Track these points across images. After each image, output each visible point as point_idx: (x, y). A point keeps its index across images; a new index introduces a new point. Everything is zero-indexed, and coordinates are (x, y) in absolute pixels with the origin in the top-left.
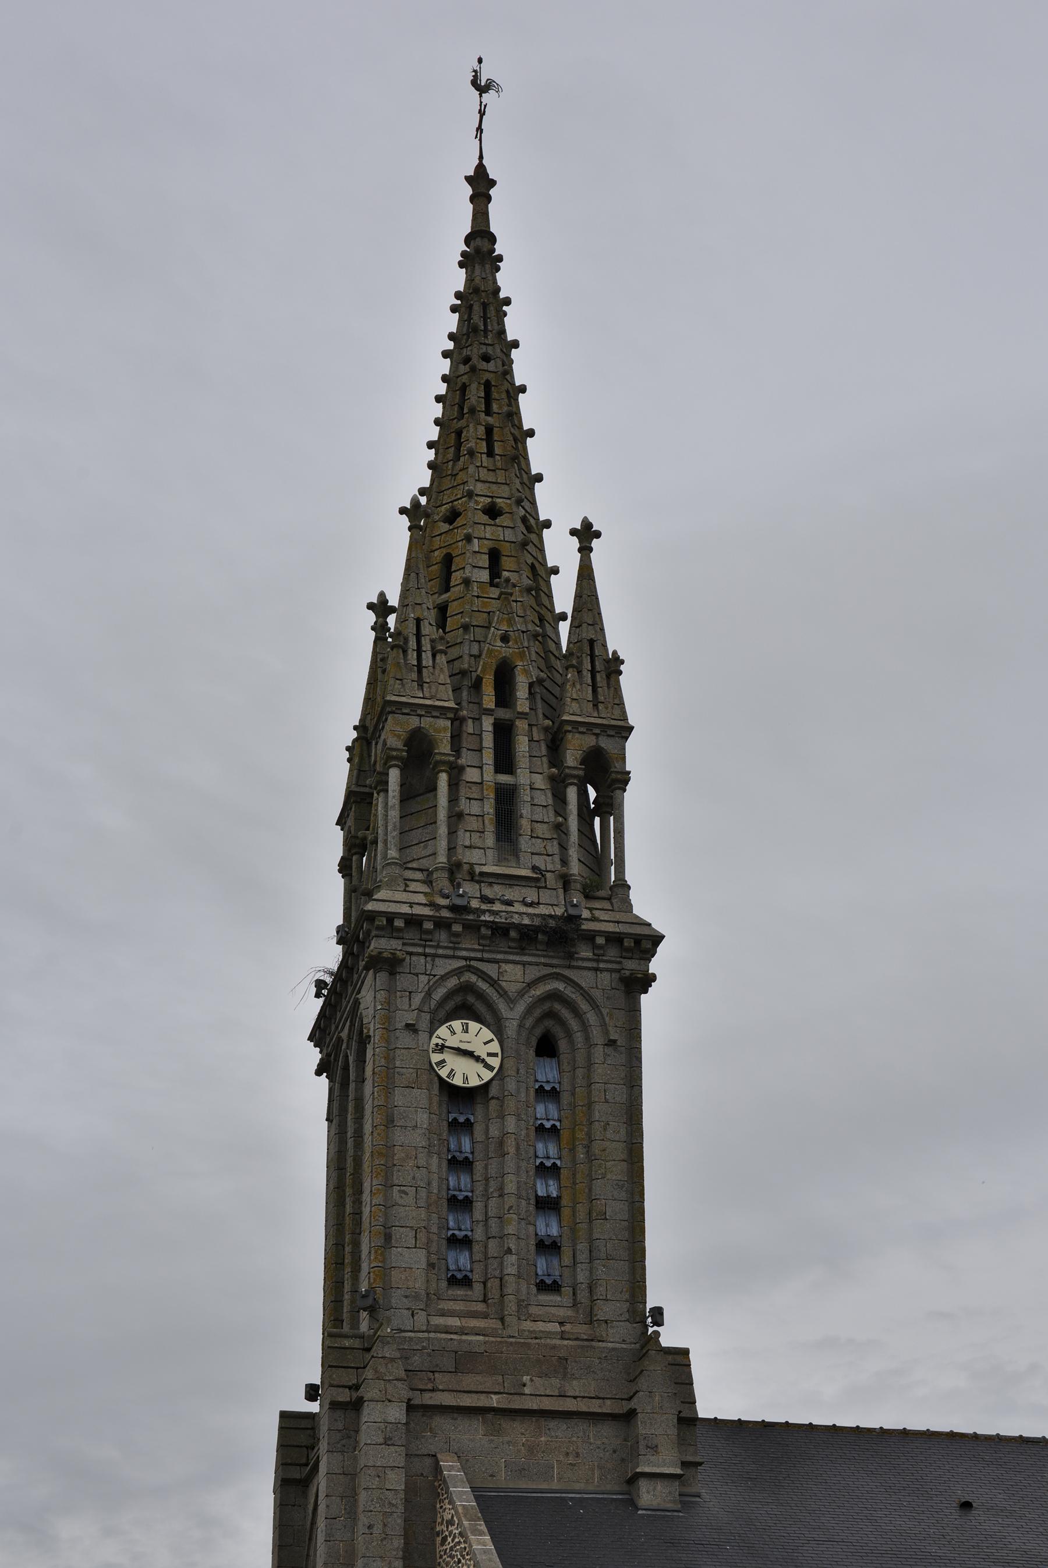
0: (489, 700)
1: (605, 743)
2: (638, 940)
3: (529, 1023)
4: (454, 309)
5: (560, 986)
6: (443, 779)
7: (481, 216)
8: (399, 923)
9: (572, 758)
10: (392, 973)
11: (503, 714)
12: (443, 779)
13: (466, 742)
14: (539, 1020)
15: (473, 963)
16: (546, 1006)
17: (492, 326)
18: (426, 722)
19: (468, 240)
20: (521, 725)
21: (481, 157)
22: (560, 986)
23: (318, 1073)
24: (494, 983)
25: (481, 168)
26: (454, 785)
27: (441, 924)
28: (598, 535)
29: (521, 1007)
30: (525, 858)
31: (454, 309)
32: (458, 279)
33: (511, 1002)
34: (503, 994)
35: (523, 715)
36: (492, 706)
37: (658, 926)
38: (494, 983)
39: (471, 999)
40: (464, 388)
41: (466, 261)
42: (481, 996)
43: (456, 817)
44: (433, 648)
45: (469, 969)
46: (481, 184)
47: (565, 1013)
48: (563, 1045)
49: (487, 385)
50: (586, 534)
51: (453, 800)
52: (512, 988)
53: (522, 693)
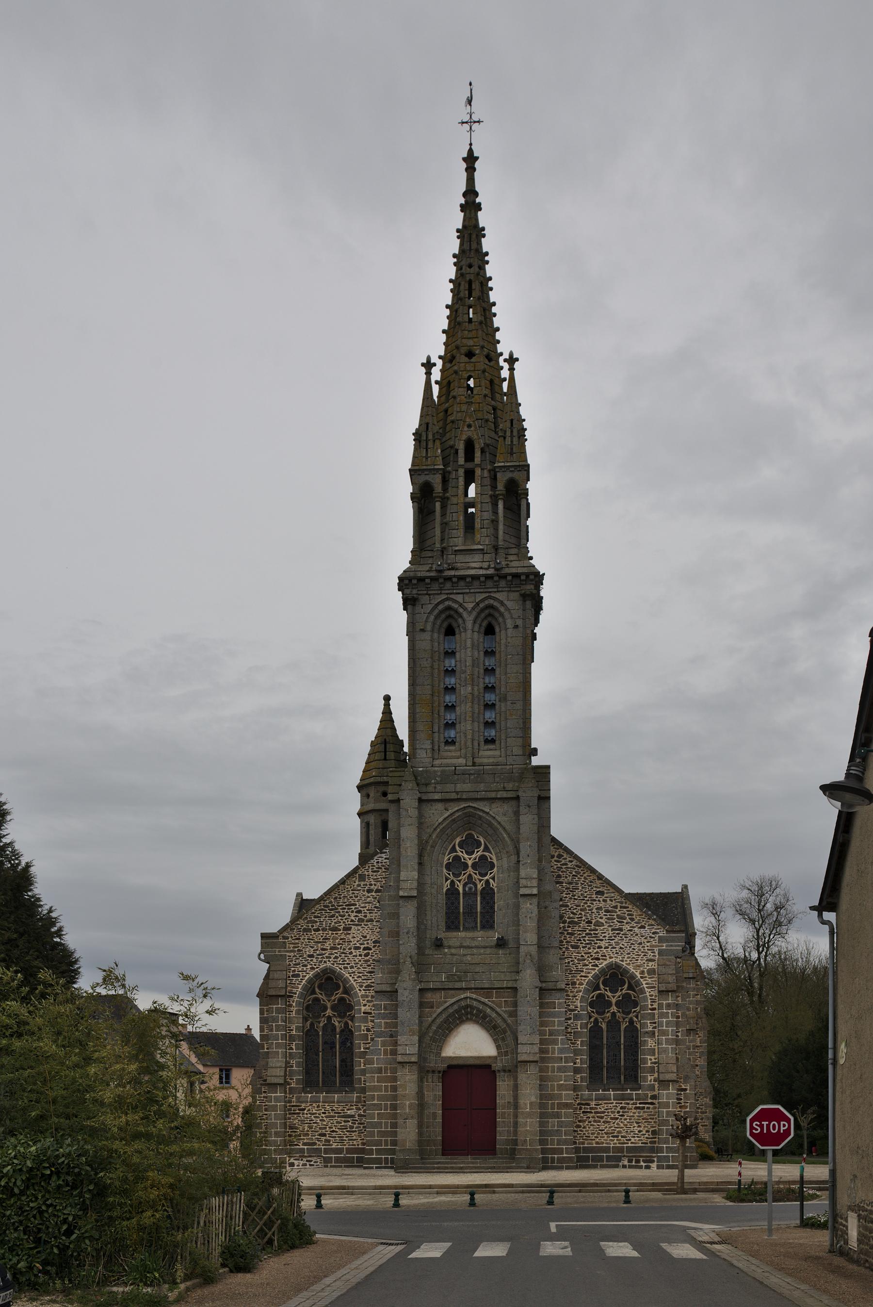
0: (461, 460)
1: (516, 475)
4: (487, 254)
5: (491, 602)
7: (471, 180)
8: (415, 581)
9: (500, 486)
10: (414, 605)
11: (470, 465)
13: (452, 483)
14: (486, 618)
15: (451, 596)
16: (487, 612)
17: (474, 246)
18: (429, 478)
19: (464, 195)
21: (471, 144)
23: (544, 574)
24: (461, 605)
25: (471, 151)
26: (444, 507)
27: (433, 579)
28: (517, 360)
30: (478, 536)
31: (487, 254)
32: (458, 219)
33: (470, 613)
34: (465, 609)
36: (463, 463)
38: (461, 605)
39: (452, 613)
40: (459, 284)
42: (456, 611)
43: (445, 525)
44: (433, 437)
45: (447, 599)
46: (471, 160)
48: (497, 630)
49: (470, 283)
50: (512, 360)
51: (443, 515)
53: (478, 454)
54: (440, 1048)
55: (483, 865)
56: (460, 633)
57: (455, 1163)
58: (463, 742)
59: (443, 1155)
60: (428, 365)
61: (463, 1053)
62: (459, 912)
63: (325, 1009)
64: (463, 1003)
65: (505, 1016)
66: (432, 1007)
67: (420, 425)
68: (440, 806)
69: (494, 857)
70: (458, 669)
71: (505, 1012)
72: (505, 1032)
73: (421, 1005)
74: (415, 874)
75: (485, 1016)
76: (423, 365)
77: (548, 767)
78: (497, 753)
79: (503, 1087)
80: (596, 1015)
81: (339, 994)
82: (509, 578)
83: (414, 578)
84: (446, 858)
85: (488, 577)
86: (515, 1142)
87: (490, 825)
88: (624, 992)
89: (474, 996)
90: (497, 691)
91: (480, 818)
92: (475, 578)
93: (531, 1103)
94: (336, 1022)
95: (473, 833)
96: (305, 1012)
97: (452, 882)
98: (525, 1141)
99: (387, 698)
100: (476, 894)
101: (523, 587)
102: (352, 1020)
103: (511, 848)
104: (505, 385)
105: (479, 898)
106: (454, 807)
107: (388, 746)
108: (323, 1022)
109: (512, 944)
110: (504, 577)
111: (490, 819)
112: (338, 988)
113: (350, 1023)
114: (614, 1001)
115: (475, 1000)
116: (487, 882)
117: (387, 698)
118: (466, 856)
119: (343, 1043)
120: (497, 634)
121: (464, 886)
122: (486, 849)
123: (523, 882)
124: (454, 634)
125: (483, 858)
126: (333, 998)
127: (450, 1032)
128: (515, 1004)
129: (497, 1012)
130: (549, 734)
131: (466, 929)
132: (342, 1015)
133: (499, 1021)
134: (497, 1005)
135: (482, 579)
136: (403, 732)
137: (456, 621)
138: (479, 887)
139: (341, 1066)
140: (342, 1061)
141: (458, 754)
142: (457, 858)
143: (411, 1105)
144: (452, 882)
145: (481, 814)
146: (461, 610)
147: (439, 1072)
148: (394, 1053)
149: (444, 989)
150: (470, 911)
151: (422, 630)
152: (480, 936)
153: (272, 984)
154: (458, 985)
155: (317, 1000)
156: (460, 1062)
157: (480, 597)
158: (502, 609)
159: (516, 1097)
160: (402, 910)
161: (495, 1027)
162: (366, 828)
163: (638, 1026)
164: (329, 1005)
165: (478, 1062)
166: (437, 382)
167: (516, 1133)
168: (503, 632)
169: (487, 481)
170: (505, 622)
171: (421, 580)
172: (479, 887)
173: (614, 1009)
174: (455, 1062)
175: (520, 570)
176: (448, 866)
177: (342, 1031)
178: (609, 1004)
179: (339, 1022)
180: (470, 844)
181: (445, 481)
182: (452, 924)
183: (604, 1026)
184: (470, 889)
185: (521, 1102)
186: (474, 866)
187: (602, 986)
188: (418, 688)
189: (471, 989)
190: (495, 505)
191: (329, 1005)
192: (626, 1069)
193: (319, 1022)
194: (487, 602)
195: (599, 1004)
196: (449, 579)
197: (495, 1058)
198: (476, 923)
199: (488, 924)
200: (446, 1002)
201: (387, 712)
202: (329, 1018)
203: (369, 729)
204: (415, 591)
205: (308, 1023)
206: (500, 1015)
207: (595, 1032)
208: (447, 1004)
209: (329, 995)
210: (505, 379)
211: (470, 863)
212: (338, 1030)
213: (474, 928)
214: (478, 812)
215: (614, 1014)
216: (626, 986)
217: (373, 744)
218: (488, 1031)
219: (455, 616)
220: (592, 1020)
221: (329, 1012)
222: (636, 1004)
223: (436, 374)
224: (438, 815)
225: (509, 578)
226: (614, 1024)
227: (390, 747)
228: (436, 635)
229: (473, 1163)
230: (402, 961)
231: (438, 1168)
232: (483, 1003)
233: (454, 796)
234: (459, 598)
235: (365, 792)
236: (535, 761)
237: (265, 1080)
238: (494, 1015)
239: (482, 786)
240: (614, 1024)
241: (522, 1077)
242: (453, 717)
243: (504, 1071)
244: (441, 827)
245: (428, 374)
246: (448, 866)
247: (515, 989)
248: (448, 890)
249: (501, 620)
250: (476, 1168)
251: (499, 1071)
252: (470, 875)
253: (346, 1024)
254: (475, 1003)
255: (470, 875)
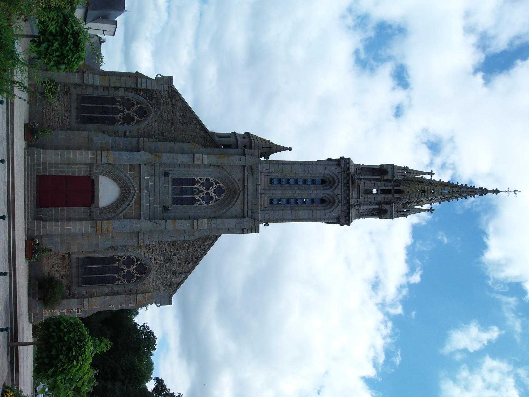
0: (395, 188)
1: (388, 214)
2: (348, 220)
3: (328, 177)
5: (337, 202)
6: (378, 177)
10: (337, 165)
12: (378, 177)
13: (386, 183)
14: (330, 200)
16: (332, 200)
19: (485, 189)
20: (390, 196)
22: (337, 202)
24: (336, 188)
25: (499, 192)
29: (332, 194)
30: (364, 195)
34: (334, 190)
35: (393, 196)
37: (351, 225)
38: (336, 188)
39: (332, 183)
41: (481, 189)
42: (333, 185)
45: (339, 182)
47: (331, 205)
48: (323, 205)
51: (374, 180)
52: (335, 192)
54: (105, 175)
55: (208, 199)
56: (323, 187)
57: (31, 184)
58: (271, 188)
59: (37, 176)
60: (431, 173)
61: (101, 188)
62: (182, 185)
63: (128, 110)
64: (132, 188)
65: (124, 212)
66: (130, 171)
67: (410, 170)
68: (241, 176)
69: (212, 204)
70: (306, 186)
71: (126, 212)
72: (114, 212)
73: (131, 165)
74: (205, 162)
75: (123, 200)
76: (432, 171)
77: (258, 232)
78: (266, 206)
79: (80, 211)
80: (122, 260)
81: (137, 118)
82: (347, 211)
83: (349, 166)
84: (212, 179)
85: (348, 201)
86: (45, 220)
87: (230, 202)
88: (136, 275)
89: (136, 195)
90: (295, 205)
91: (234, 197)
92: (348, 195)
93: (70, 229)
94: (121, 115)
95: (225, 193)
96: (127, 98)
97: (198, 182)
98: (46, 226)
99: (290, 149)
100: (192, 194)
101: (343, 218)
102: (121, 124)
103: (218, 214)
104: (419, 207)
105: (190, 196)
106: (240, 184)
107: (268, 149)
108: (121, 108)
109: (166, 215)
110: (348, 209)
111: (233, 202)
112: (141, 117)
113: (120, 123)
114: (131, 269)
115: (134, 196)
116: (199, 201)
117: (290, 149)
118: (213, 189)
119: (107, 118)
120: (322, 205)
121: (197, 188)
122: (217, 200)
123: (200, 221)
124: (322, 184)
125: (212, 198)
126: (134, 114)
127: (115, 181)
128: (130, 219)
129: (126, 208)
130: (272, 232)
131: (173, 189)
132: (124, 119)
133: (121, 209)
134: (130, 208)
135: (348, 198)
136: (273, 157)
137: (329, 185)
138: (196, 197)
139: (94, 116)
140: (97, 118)
141: (266, 186)
142: (212, 185)
143: (69, 158)
144: (198, 182)
145: (236, 198)
146: (334, 188)
147: (90, 174)
148: (102, 149)
149: (140, 178)
150: (182, 192)
151: (326, 169)
152: (169, 198)
153: (144, 80)
154: (142, 186)
155: (133, 105)
156: (95, 187)
157: (339, 196)
158: (333, 208)
159: (74, 220)
160: (186, 155)
161: (117, 207)
162: (227, 136)
163: (116, 283)
164: (130, 112)
165: (96, 196)
166: (422, 177)
167: (51, 220)
168: (322, 208)
169: (386, 200)
170: (327, 209)
171: (348, 169)
172: (196, 197)
173: (126, 270)
174: (95, 183)
175: (350, 216)
176: (208, 180)
177: (115, 118)
178: (129, 267)
179: (120, 117)
180: (219, 191)
181: (387, 180)
182: (176, 182)
183: (116, 265)
184: (195, 191)
185: (71, 223)
186: (208, 194)
187: (139, 262)
188: (299, 166)
189: (140, 193)
190: (377, 204)
191: (130, 112)
192: (90, 278)
193: (120, 106)
194: (337, 200)
195: (129, 262)
196: (348, 183)
197: (98, 206)
198: (176, 195)
199: (176, 201)
200: (133, 179)
201: (283, 149)
202: (123, 112)
203: (275, 140)
204: (343, 165)
205: (120, 100)
206: (124, 209)
207: (113, 260)
208: (131, 180)
209: (136, 112)
210: (422, 206)
211: (209, 191)
212: (115, 116)
213: (174, 194)
214: (237, 196)
215: (123, 270)
216: (139, 276)
217: (269, 141)
218: (115, 202)
219: (331, 185)
220: (120, 258)
221: (126, 111)
222: (129, 281)
223: (428, 177)
224: (237, 175)
225: (347, 211)
226: (117, 270)
227: (268, 150)
228: (323, 175)
229: (31, 195)
230: (157, 154)
231: (28, 175)
232: (132, 200)
233: (246, 184)
234: (339, 187)
235: (246, 136)
236: (262, 226)
237: (85, 72)
238: (124, 206)
239: (250, 198)
240: (117, 270)
241: (88, 223)
242: (283, 183)
243: (90, 212)
244: (230, 177)
245: (428, 174)
246: (208, 180)
247: (140, 218)
248: (195, 179)
249: (328, 207)
250: (28, 198)
251: (90, 209)
252: (203, 191)
253: (119, 121)
254: (131, 195)
255: (203, 191)
